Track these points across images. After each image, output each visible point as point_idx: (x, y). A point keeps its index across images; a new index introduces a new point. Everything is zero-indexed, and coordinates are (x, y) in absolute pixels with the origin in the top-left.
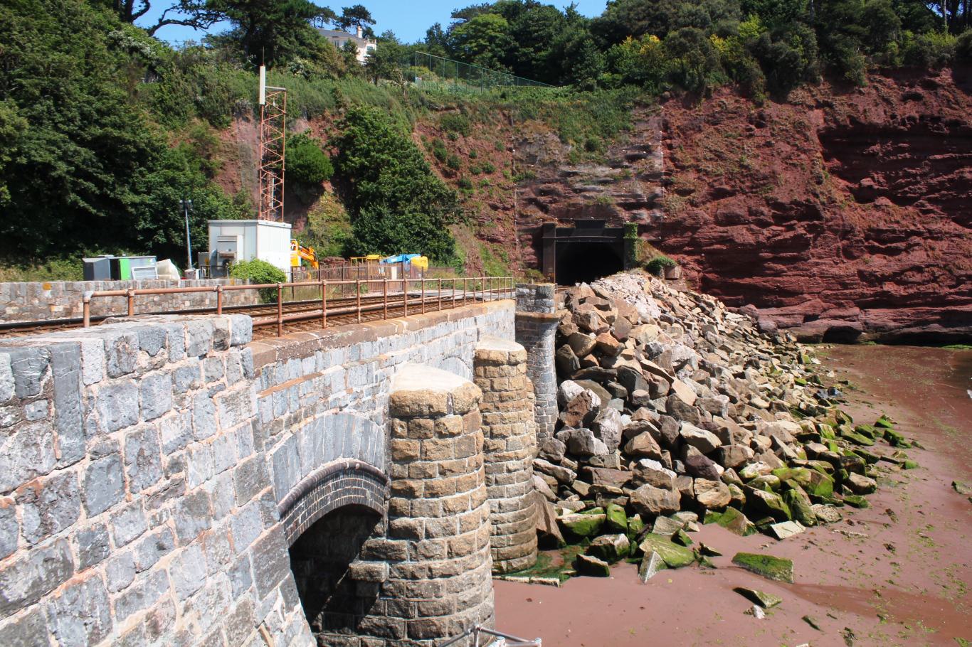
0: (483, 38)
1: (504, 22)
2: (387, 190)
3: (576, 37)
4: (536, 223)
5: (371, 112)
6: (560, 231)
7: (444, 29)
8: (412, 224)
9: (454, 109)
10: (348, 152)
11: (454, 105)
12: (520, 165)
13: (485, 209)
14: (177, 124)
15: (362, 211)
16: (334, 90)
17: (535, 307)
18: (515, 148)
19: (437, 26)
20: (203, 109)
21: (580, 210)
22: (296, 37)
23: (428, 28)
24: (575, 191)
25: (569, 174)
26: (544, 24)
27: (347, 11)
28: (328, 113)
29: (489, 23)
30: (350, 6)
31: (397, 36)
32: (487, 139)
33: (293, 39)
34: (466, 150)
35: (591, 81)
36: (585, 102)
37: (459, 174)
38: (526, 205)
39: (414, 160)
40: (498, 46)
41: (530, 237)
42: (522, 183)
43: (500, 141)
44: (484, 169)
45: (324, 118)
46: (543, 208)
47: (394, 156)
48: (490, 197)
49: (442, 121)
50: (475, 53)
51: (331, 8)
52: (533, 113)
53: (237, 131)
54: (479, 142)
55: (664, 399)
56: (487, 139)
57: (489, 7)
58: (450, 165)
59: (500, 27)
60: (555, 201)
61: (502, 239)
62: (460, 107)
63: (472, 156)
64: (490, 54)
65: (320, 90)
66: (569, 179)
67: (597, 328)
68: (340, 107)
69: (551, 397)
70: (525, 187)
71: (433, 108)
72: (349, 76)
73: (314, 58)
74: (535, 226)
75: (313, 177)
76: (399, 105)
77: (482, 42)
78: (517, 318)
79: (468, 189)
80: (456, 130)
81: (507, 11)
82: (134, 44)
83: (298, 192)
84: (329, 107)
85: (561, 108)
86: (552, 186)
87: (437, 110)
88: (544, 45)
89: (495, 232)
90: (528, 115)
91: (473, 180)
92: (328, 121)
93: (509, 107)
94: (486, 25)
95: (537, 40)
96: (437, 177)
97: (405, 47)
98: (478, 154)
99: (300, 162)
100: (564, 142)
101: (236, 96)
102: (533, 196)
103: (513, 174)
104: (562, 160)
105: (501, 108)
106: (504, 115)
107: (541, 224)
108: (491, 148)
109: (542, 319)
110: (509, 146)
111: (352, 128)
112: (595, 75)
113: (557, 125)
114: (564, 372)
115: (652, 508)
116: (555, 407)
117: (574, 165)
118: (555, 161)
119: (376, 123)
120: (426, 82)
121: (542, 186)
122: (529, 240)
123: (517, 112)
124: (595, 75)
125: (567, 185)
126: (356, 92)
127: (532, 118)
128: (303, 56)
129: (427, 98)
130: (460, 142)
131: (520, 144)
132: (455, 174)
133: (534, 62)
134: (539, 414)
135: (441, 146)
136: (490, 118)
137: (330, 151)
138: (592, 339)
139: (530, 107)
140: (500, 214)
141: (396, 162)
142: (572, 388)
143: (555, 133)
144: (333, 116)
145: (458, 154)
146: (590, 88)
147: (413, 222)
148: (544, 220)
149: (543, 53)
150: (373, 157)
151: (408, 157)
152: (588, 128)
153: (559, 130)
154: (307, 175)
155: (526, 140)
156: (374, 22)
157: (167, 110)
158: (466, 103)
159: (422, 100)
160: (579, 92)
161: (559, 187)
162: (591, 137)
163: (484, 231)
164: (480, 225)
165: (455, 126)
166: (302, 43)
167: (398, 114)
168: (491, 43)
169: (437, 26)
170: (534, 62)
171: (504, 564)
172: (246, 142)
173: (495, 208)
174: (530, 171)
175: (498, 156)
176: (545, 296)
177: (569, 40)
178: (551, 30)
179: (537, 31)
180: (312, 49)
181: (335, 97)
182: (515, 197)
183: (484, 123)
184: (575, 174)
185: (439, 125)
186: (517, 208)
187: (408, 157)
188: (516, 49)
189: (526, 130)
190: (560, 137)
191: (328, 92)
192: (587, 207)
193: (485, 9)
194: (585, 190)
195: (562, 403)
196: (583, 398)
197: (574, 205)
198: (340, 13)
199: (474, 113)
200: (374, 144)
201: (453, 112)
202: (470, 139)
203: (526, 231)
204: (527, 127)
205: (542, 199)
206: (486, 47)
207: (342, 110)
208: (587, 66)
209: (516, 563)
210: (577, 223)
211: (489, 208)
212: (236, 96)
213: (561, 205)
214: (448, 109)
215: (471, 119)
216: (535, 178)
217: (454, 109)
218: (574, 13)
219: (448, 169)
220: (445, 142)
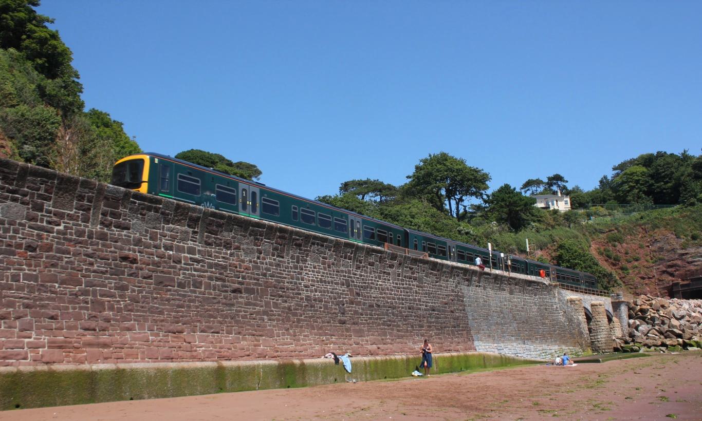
0: (632, 182)
1: (644, 169)
3: (686, 172)
4: (669, 283)
5: (568, 242)
6: (683, 286)
7: (609, 178)
9: (613, 230)
10: (560, 262)
11: (613, 228)
12: (655, 254)
13: (637, 280)
16: (551, 235)
17: (617, 299)
18: (651, 245)
19: (605, 177)
21: (692, 273)
22: (530, 213)
23: (600, 179)
24: (688, 263)
25: (683, 254)
26: (668, 167)
27: (549, 179)
28: (549, 246)
29: (634, 173)
30: (551, 175)
31: (581, 188)
32: (633, 243)
33: (528, 214)
34: (623, 251)
35: (693, 200)
36: (689, 213)
37: (620, 264)
38: (661, 275)
39: (590, 261)
40: (642, 185)
41: (666, 291)
42: (657, 263)
43: (641, 243)
44: (634, 259)
45: (548, 248)
46: (672, 275)
47: (581, 261)
48: (639, 273)
49: (608, 237)
50: (628, 191)
51: (540, 179)
52: (658, 225)
54: (629, 246)
55: (667, 325)
56: (633, 243)
57: (635, 160)
58: (615, 259)
59: (641, 173)
60: (677, 270)
62: (616, 229)
64: (637, 191)
65: (544, 236)
66: (684, 257)
67: (640, 304)
68: (554, 242)
69: (625, 324)
70: (659, 265)
72: (556, 227)
73: (539, 221)
74: (668, 285)
76: (581, 235)
77: (631, 184)
78: (612, 303)
79: (626, 270)
80: (615, 241)
81: (645, 162)
82: (467, 231)
85: (674, 219)
86: (674, 262)
87: (604, 233)
88: (670, 179)
90: (655, 227)
91: (629, 265)
92: (550, 249)
93: (644, 224)
94: (632, 174)
95: (664, 177)
96: (606, 267)
97: (588, 193)
98: (630, 252)
100: (678, 237)
101: (509, 245)
102: (665, 269)
104: (678, 247)
105: (640, 225)
106: (642, 228)
107: (671, 283)
108: (637, 247)
109: (619, 302)
110: (647, 245)
111: (561, 251)
112: (695, 196)
113: (673, 229)
114: (630, 317)
115: (650, 345)
116: (627, 327)
118: (674, 248)
119: (571, 248)
120: (603, 217)
121: (669, 263)
122: (666, 293)
123: (650, 226)
124: (695, 196)
125: (682, 260)
126: (561, 234)
127: (658, 227)
128: (534, 222)
129: (597, 227)
130: (619, 246)
131: (653, 243)
132: (618, 264)
133: (665, 191)
134: (622, 329)
135: (609, 251)
136: (634, 232)
137: (553, 262)
138: (638, 308)
139: (657, 221)
140: (647, 281)
141: (582, 263)
142: (631, 321)
143: (672, 233)
144: (552, 247)
145: (618, 253)
146: (692, 204)
148: (673, 281)
149: (669, 185)
151: (587, 260)
152: (692, 227)
153: (675, 231)
155: (656, 240)
156: (567, 182)
158: (620, 226)
159: (595, 229)
160: (686, 207)
161: (679, 262)
162: (694, 232)
164: (635, 288)
165: (615, 239)
166: (533, 216)
167: (582, 241)
168: (637, 184)
169: (605, 177)
170: (665, 191)
171: (603, 351)
173: (643, 278)
174: (661, 256)
175: (641, 251)
176: (619, 295)
177: (682, 175)
178: (673, 170)
179: (663, 172)
180: (538, 217)
182: (655, 271)
183: (631, 235)
184: (687, 254)
185: (606, 240)
186: (656, 277)
187: (587, 260)
188: (652, 185)
189: (655, 235)
190: (676, 235)
191: (548, 236)
192: (697, 270)
193: (632, 162)
194: (694, 262)
195: (629, 325)
196: (634, 323)
197: (688, 271)
198: (546, 180)
199: (625, 231)
200: (571, 257)
201: (613, 232)
202: (624, 245)
203: (664, 288)
204: (656, 233)
205: (669, 270)
206: (634, 187)
207: (555, 243)
208: (689, 192)
209: (606, 351)
210: (692, 280)
211: (640, 279)
212: (509, 245)
213: (682, 271)
214: (610, 231)
215: (623, 234)
216: (664, 259)
217: (613, 230)
218: (686, 156)
219: (614, 262)
220: (611, 248)
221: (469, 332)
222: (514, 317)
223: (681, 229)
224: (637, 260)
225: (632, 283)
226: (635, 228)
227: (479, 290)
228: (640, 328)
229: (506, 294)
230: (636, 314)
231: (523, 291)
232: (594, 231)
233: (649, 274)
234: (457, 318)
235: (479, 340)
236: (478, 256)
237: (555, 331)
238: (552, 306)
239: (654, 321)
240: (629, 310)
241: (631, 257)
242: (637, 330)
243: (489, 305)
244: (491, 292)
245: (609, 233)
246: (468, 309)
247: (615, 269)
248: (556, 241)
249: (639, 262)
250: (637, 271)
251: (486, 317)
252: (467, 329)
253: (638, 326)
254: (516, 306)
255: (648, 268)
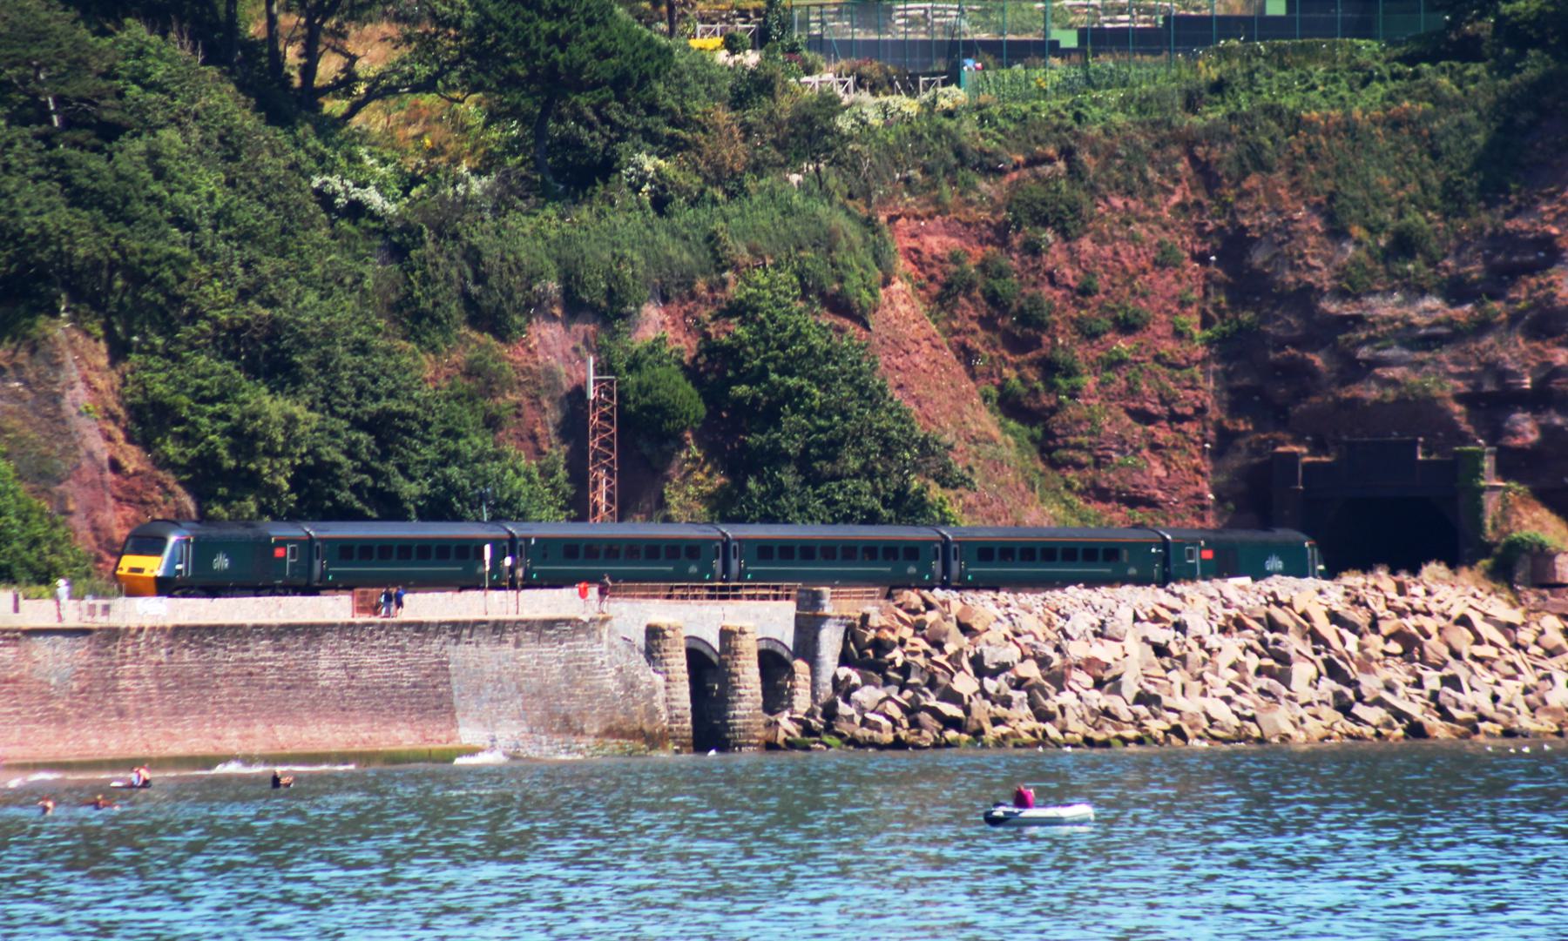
2: (792, 447)
8: (836, 502)
11: (1051, 151)
14: (438, 338)
15: (752, 484)
20: (478, 308)
28: (701, 285)
32: (1133, 238)
37: (1046, 339)
45: (693, 296)
53: (536, 341)
54: (1107, 251)
61: (1160, 495)
62: (1067, 153)
63: (1086, 291)
68: (724, 269)
71: (990, 167)
75: (668, 425)
78: (797, 616)
79: (1067, 376)
83: (646, 449)
84: (704, 273)
89: (1138, 479)
91: (1081, 353)
98: (1101, 283)
99: (647, 400)
103: (1206, 323)
104: (1327, 285)
114: (845, 660)
117: (1357, 297)
135: (1001, 274)
136: (1151, 173)
138: (871, 635)
140: (1162, 434)
142: (844, 672)
147: (839, 497)
150: (771, 384)
154: (661, 422)
157: (418, 316)
159: (959, 152)
163: (1107, 478)
172: (553, 361)
181: (713, 250)
196: (848, 678)
199: (1105, 167)
201: (1046, 170)
202: (1086, 244)
207: (727, 274)
214: (1033, 162)
217: (1049, 160)
220: (1013, 262)
221: (453, 716)
222: (519, 688)
223: (1359, 194)
224: (1127, 327)
225: (1085, 440)
226: (1157, 155)
227: (470, 648)
228: (856, 695)
229: (508, 649)
230: (862, 654)
231: (540, 638)
232: (954, 161)
233: (1175, 399)
234: (440, 696)
235: (467, 726)
236: (296, 90)
237: (593, 708)
238: (593, 659)
239: (907, 676)
240: (845, 642)
241: (1101, 306)
242: (847, 700)
243: (482, 672)
244: (485, 649)
245: (1026, 173)
246: (454, 680)
247: (1017, 367)
248: (736, 267)
249: (1139, 337)
250: (1119, 382)
251: (477, 691)
252: (451, 711)
253: (855, 688)
254: (524, 668)
255: (1180, 368)
